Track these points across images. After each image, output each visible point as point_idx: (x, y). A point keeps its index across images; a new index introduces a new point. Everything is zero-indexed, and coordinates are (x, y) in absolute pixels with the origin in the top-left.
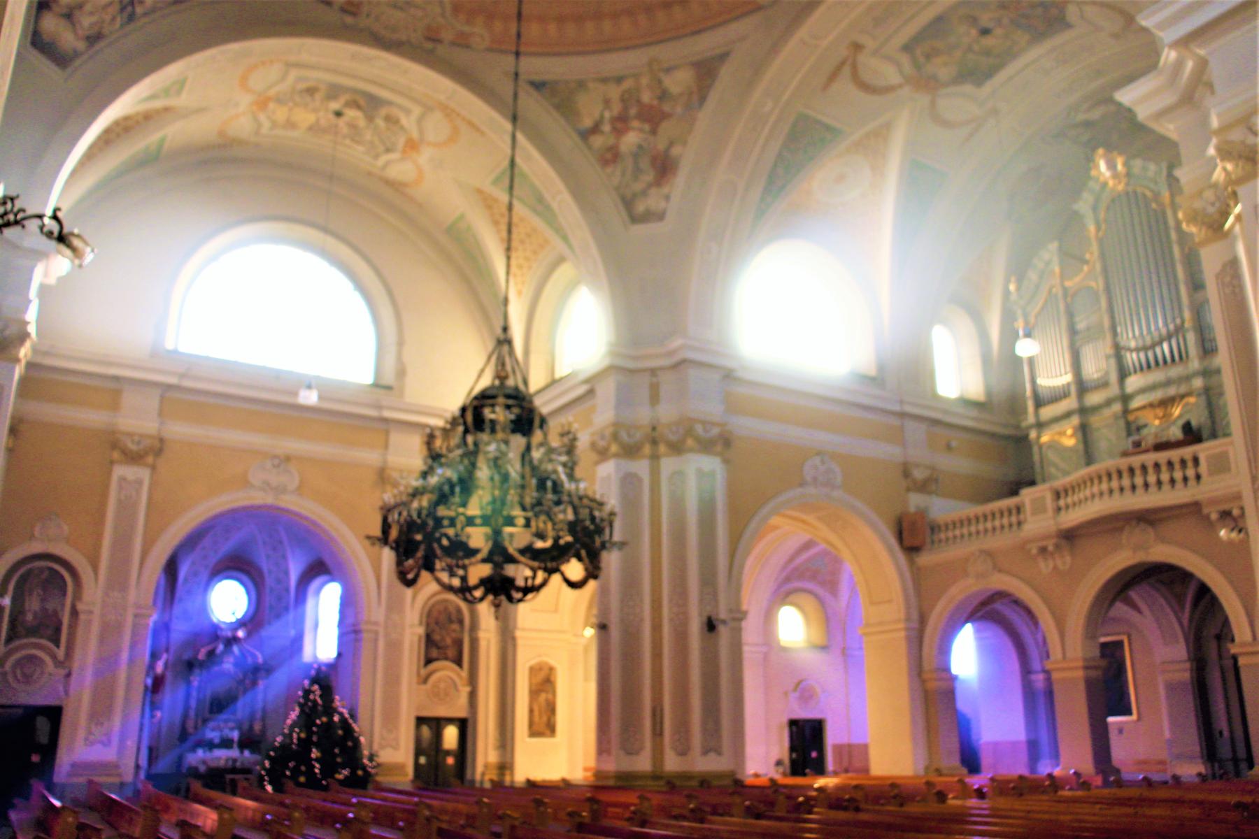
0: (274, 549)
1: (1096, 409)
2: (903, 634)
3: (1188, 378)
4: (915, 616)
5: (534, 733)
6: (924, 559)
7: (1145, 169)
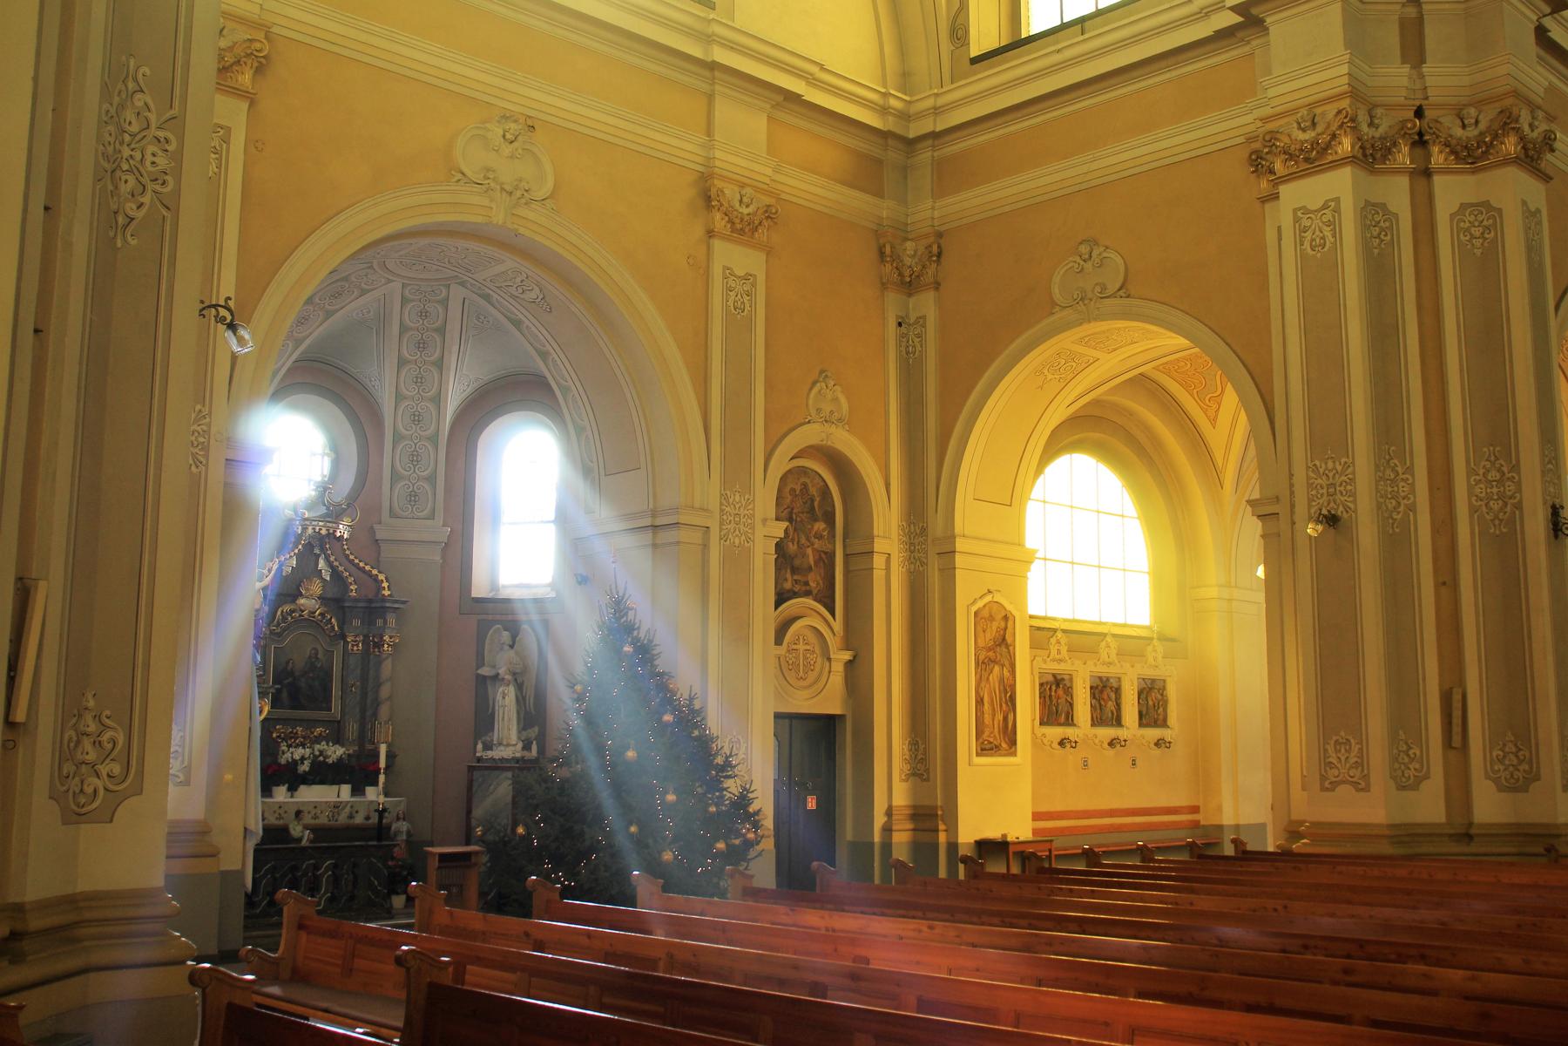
0: (422, 345)
5: (985, 749)
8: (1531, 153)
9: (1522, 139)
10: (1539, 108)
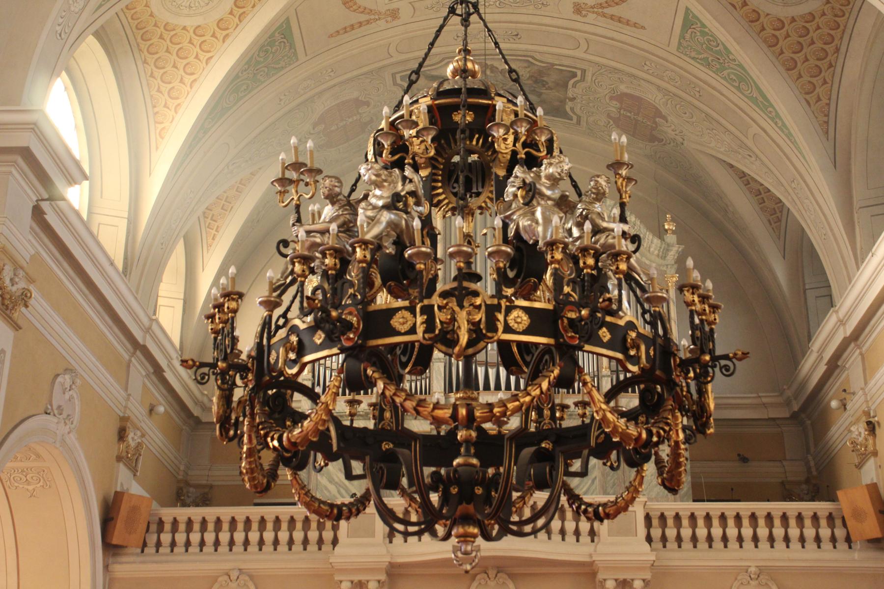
8: (7, 302)
9: (405, 400)
10: (22, 268)
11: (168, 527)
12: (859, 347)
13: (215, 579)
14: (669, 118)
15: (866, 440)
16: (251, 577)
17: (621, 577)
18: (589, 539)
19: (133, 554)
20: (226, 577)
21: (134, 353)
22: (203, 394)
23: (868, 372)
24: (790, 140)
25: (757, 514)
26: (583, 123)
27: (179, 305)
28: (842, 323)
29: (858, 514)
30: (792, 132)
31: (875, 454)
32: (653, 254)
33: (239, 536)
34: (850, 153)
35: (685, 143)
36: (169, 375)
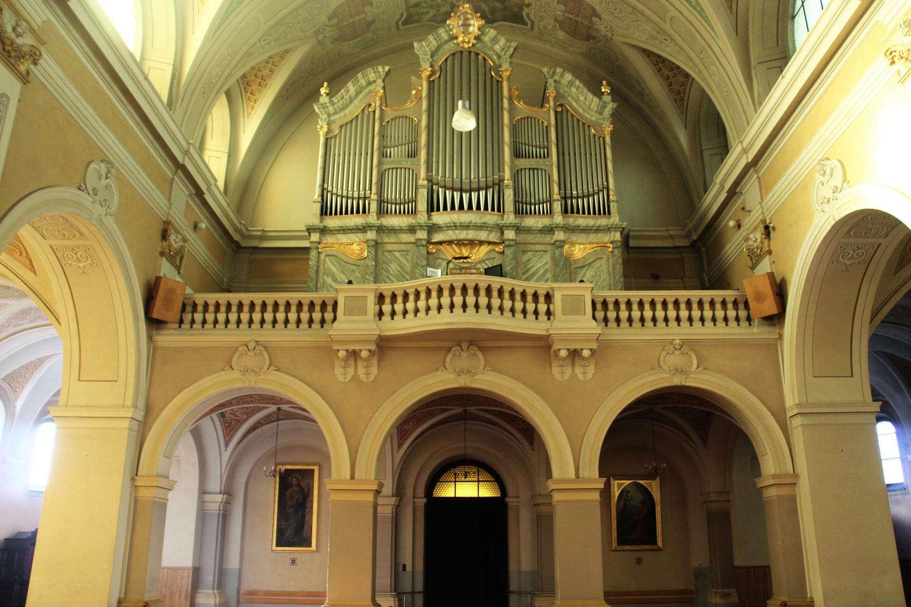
1: (393, 230)
2: (126, 424)
3: (501, 229)
4: (142, 404)
6: (168, 338)
7: (495, 40)
11: (200, 308)
12: (757, 172)
13: (236, 349)
14: (603, 16)
15: (762, 243)
16: (266, 348)
17: (573, 347)
18: (546, 317)
19: (172, 329)
20: (245, 348)
21: (176, 172)
22: (241, 224)
23: (764, 189)
24: (702, 16)
25: (680, 299)
26: (536, 28)
27: (225, 157)
28: (745, 151)
29: (759, 297)
30: (705, 9)
31: (770, 252)
32: (592, 110)
33: (257, 316)
34: (748, 24)
35: (614, 38)
36: (208, 197)
